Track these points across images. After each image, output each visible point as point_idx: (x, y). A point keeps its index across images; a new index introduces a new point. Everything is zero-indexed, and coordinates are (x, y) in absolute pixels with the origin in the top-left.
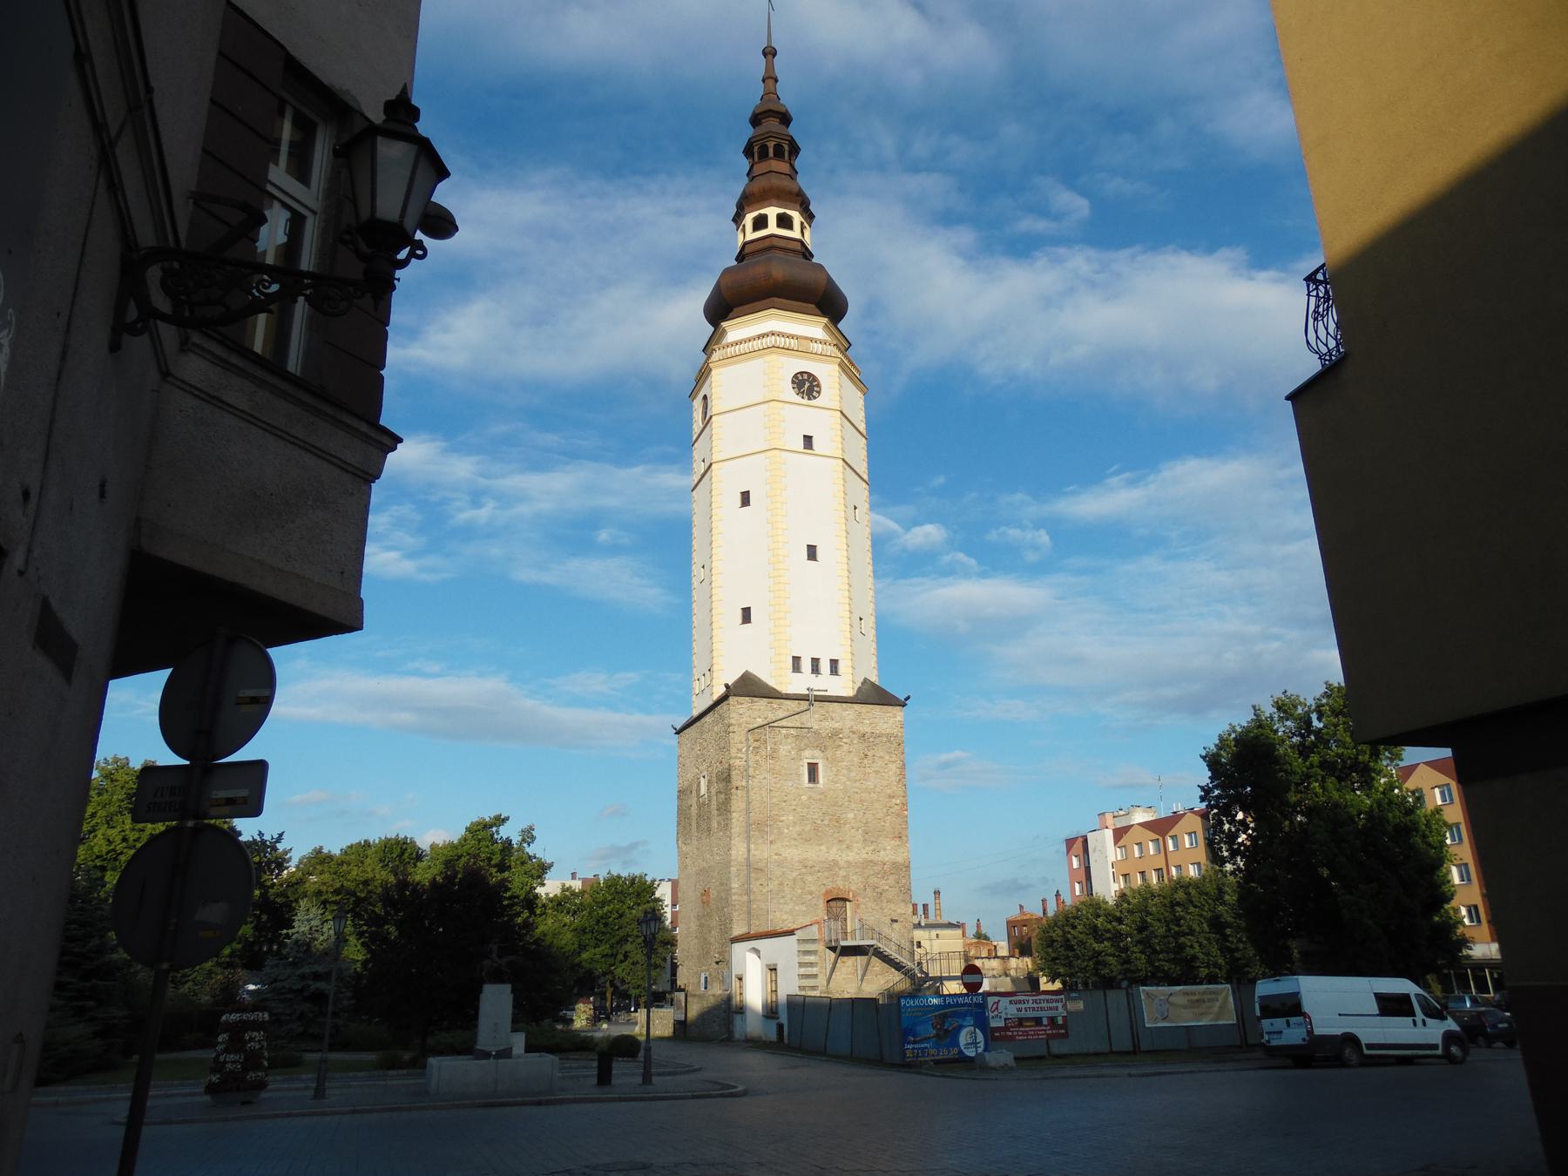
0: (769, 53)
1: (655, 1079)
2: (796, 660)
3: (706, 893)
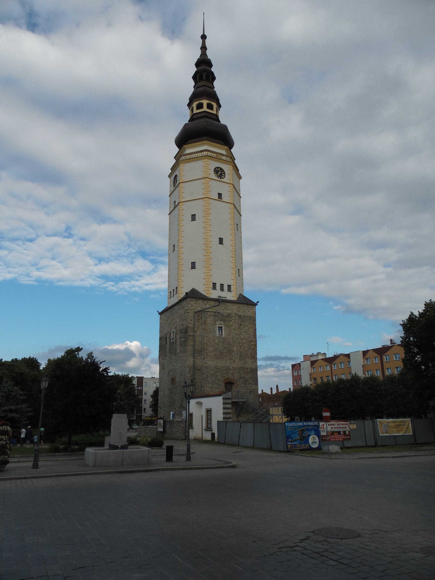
0: (204, 37)
1: (174, 458)
2: (214, 284)
3: (173, 380)
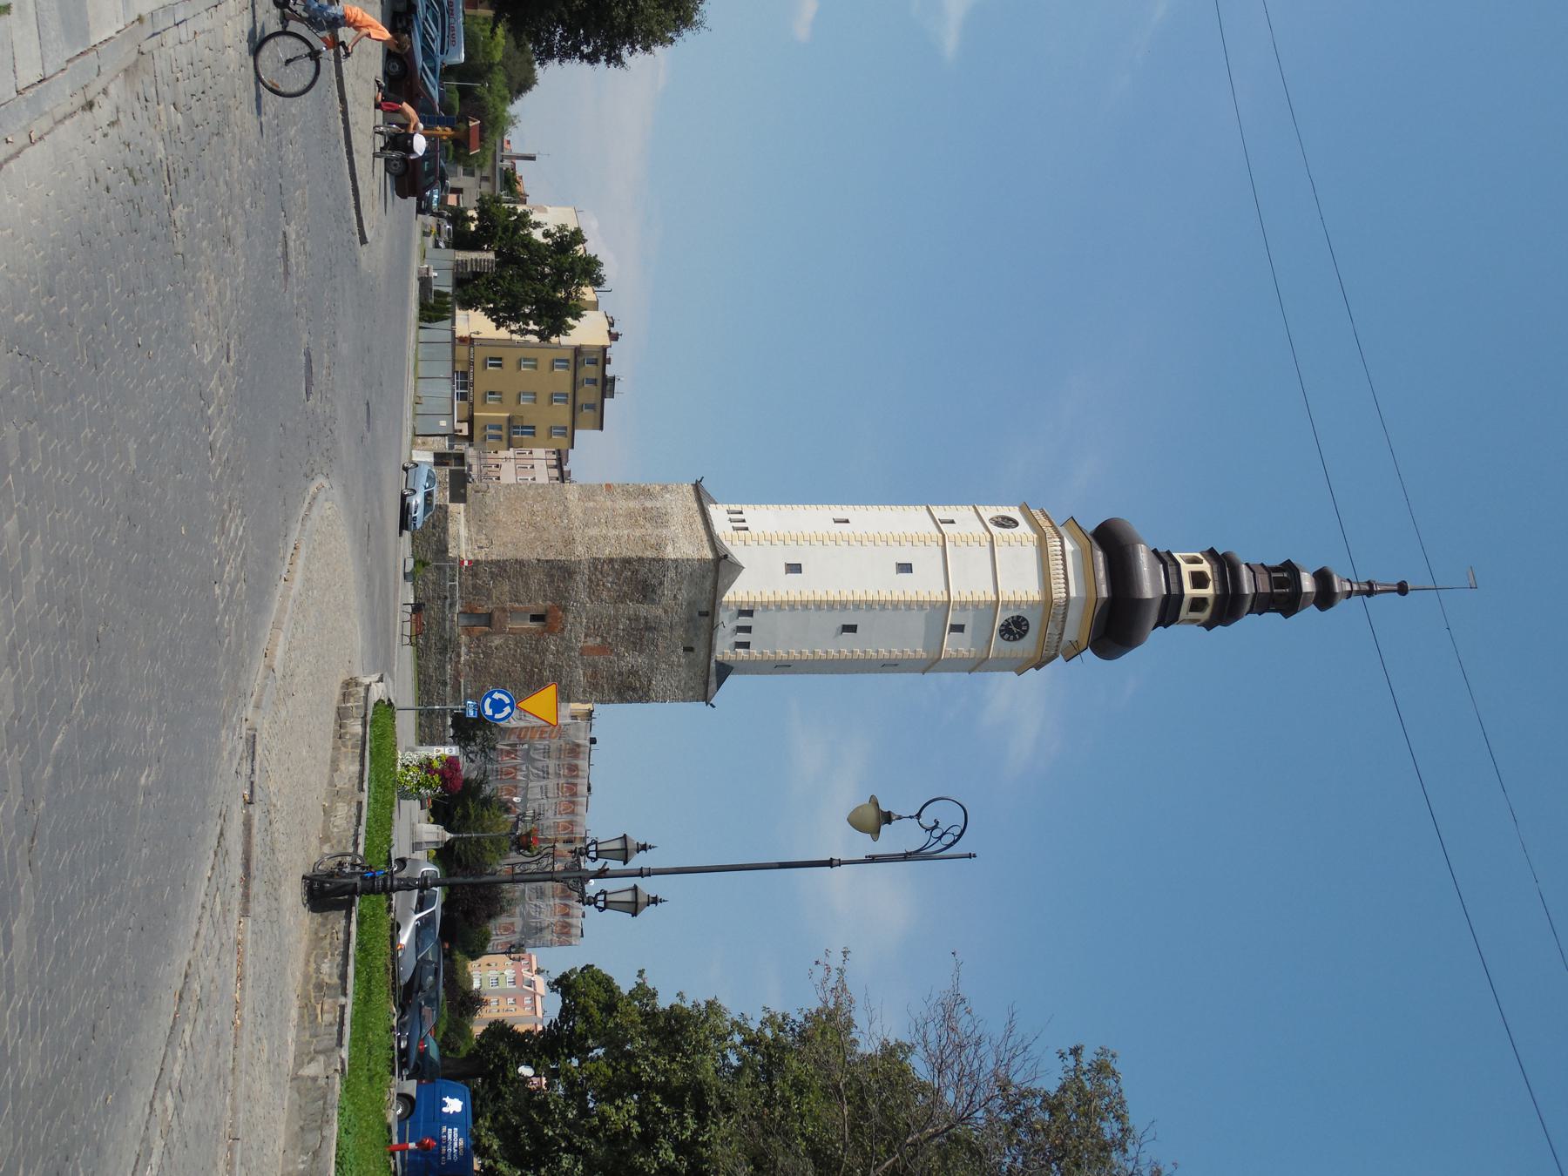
2: (750, 613)
